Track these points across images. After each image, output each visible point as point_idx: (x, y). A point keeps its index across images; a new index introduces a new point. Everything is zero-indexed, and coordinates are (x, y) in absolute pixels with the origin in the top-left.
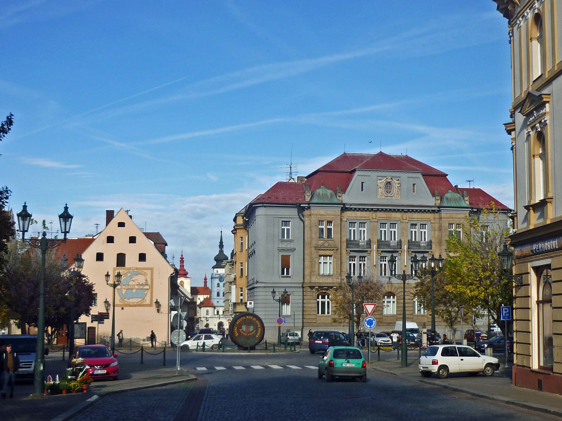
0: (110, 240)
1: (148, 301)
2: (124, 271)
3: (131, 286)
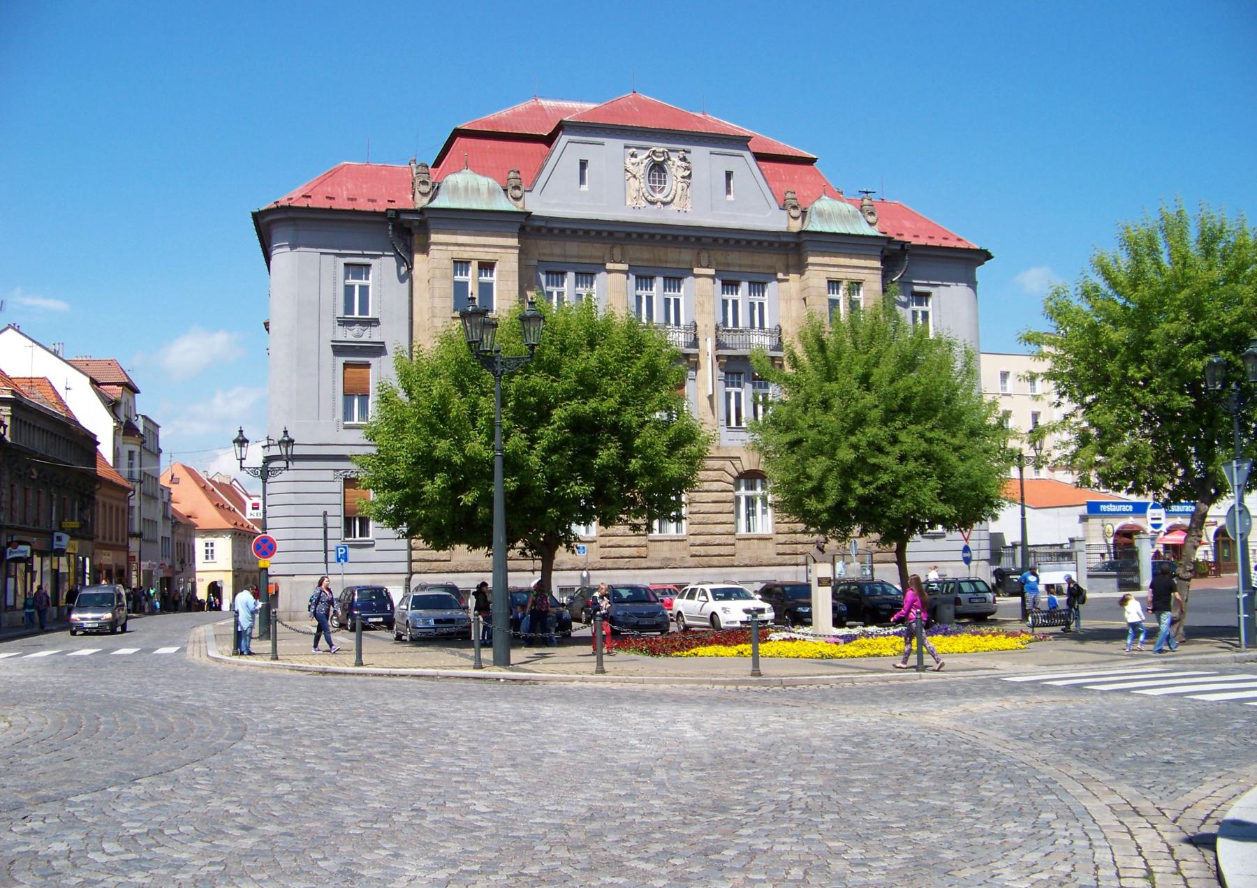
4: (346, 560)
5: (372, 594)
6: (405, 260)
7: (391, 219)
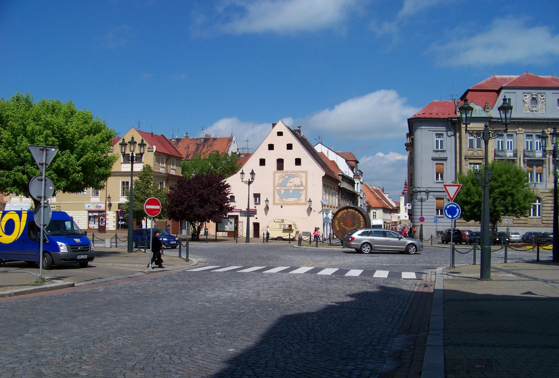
0: (271, 147)
1: (303, 201)
2: (282, 174)
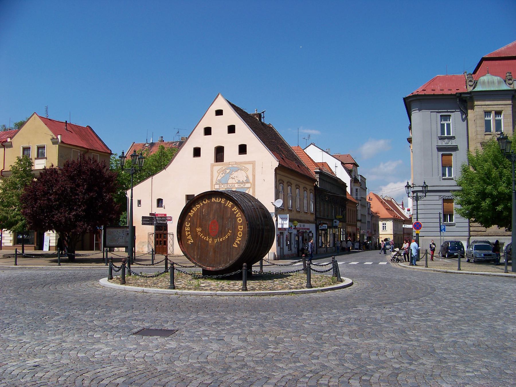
3: (230, 185)
4: (445, 231)
5: (455, 244)
6: (464, 113)
7: (458, 97)
